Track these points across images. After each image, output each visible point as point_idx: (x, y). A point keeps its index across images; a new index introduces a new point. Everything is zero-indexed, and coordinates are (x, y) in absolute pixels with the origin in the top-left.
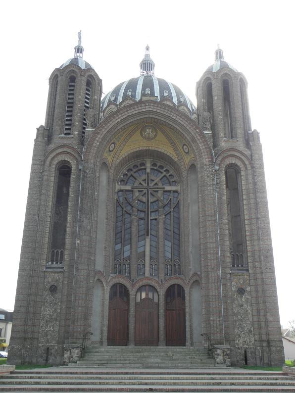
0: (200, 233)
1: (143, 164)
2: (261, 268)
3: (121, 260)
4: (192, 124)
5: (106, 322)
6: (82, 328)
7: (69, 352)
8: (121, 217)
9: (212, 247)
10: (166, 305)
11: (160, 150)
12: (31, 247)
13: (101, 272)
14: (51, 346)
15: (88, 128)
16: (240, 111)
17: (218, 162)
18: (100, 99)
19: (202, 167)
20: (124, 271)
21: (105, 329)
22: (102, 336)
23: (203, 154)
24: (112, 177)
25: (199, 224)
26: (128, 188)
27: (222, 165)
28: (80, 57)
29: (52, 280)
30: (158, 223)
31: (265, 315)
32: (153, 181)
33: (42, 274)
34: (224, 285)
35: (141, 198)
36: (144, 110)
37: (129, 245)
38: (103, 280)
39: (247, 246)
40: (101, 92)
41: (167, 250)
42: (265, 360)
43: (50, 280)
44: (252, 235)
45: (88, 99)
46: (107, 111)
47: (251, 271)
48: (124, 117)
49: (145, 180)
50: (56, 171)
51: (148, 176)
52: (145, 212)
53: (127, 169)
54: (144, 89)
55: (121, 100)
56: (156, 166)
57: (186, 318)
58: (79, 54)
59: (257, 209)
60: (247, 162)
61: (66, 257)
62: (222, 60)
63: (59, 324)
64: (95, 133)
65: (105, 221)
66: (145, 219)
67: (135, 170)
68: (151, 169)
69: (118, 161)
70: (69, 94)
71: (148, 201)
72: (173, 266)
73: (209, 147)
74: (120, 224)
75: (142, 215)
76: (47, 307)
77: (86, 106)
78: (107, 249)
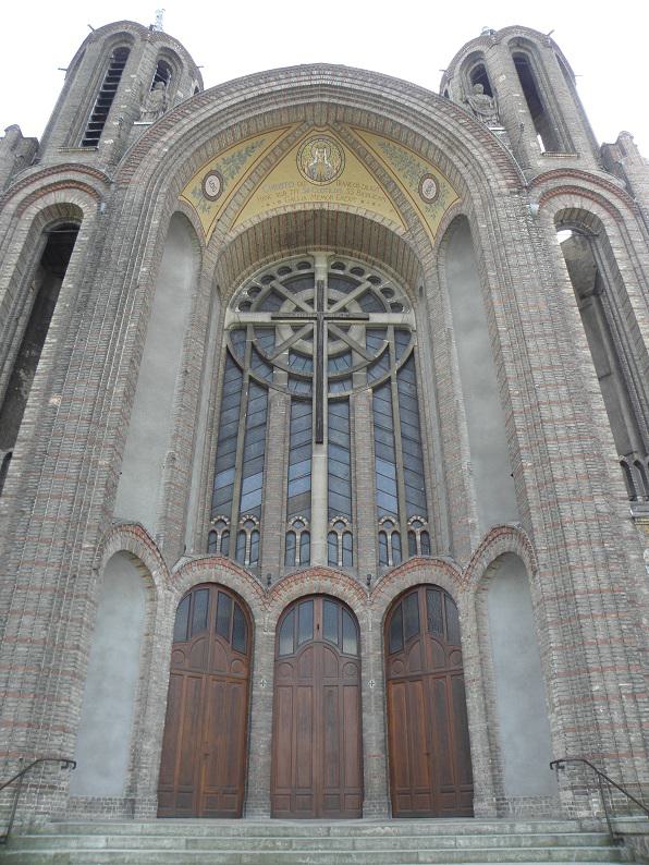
3: (230, 520)
4: (444, 109)
5: (156, 721)
6: (21, 738)
8: (237, 397)
9: (558, 416)
10: (388, 662)
11: (352, 211)
21: (152, 748)
22: (135, 780)
23: (487, 172)
26: (263, 318)
36: (308, 83)
41: (377, 485)
51: (321, 290)
53: (261, 275)
56: (342, 267)
57: (470, 704)
60: (618, 204)
65: (179, 378)
69: (234, 235)
75: (302, 390)
78: (177, 464)
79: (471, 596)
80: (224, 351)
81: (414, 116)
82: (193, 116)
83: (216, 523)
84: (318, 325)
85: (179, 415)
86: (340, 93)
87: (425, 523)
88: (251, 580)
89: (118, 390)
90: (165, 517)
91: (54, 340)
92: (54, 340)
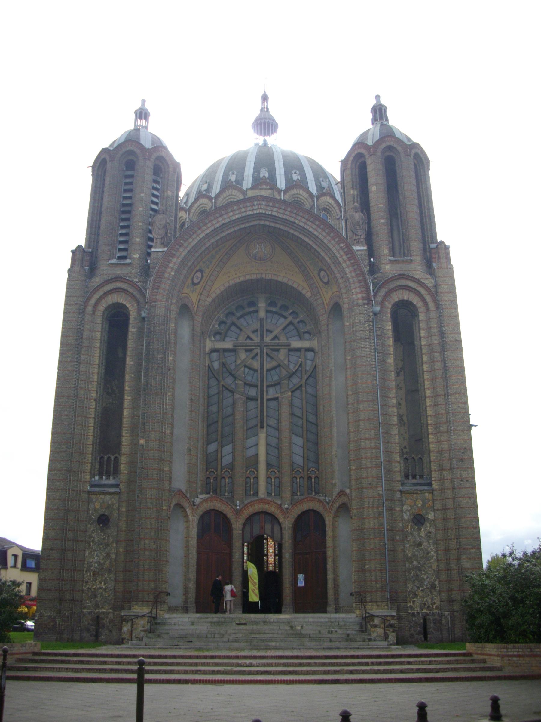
0: (348, 423)
1: (252, 304)
2: (452, 480)
3: (217, 471)
5: (193, 575)
6: (152, 585)
7: (129, 624)
11: (280, 279)
12: (65, 452)
13: (182, 492)
14: (103, 613)
15: (156, 247)
16: (415, 209)
17: (379, 299)
18: (177, 196)
19: (351, 309)
20: (223, 489)
21: (192, 586)
23: (352, 286)
24: (198, 329)
25: (347, 407)
26: (228, 345)
27: (386, 303)
28: (143, 127)
29: (101, 505)
30: (279, 406)
31: (459, 559)
32: (271, 332)
33: (84, 496)
34: (391, 510)
35: (249, 362)
36: (251, 213)
37: (231, 445)
38: (186, 505)
39: (429, 444)
40: (178, 183)
42: (456, 632)
43: (98, 505)
44: (437, 425)
45: (156, 204)
46: (194, 208)
47: (435, 485)
48: (217, 225)
49: (257, 331)
50: (104, 323)
51: (262, 326)
52: (256, 386)
53: (225, 312)
54: (257, 170)
55: (218, 190)
58: (143, 122)
59: (446, 379)
60: (428, 298)
61: (123, 468)
62: (385, 123)
63: (115, 579)
64: (168, 255)
66: (257, 400)
67: (238, 314)
68: (267, 311)
69: (210, 300)
70: (125, 191)
71: (262, 368)
72: (306, 479)
73: (362, 274)
74: (214, 408)
75: (253, 392)
76: (95, 551)
77: (153, 210)
78: (192, 453)
79: (331, 519)
80: (207, 368)
81: (314, 238)
82: (185, 245)
83: (210, 472)
84: (261, 350)
85: (191, 425)
86: (271, 218)
87: (317, 472)
88: (230, 507)
89: (168, 432)
90: (189, 481)
91: (129, 398)
92: (129, 398)
